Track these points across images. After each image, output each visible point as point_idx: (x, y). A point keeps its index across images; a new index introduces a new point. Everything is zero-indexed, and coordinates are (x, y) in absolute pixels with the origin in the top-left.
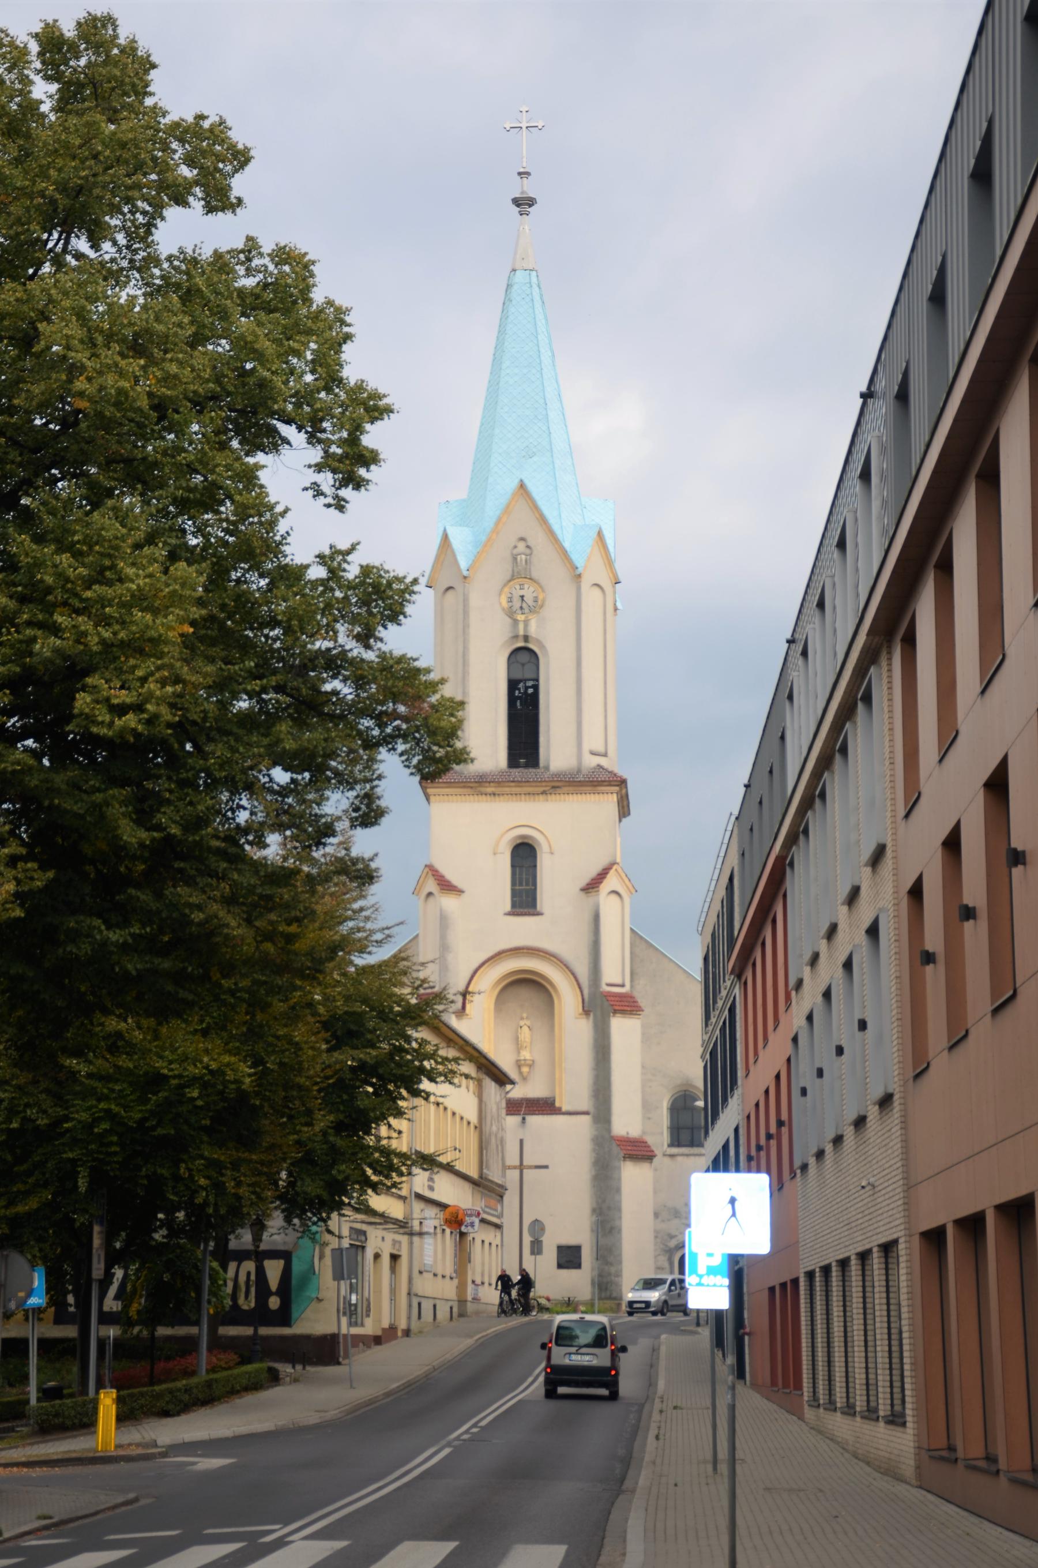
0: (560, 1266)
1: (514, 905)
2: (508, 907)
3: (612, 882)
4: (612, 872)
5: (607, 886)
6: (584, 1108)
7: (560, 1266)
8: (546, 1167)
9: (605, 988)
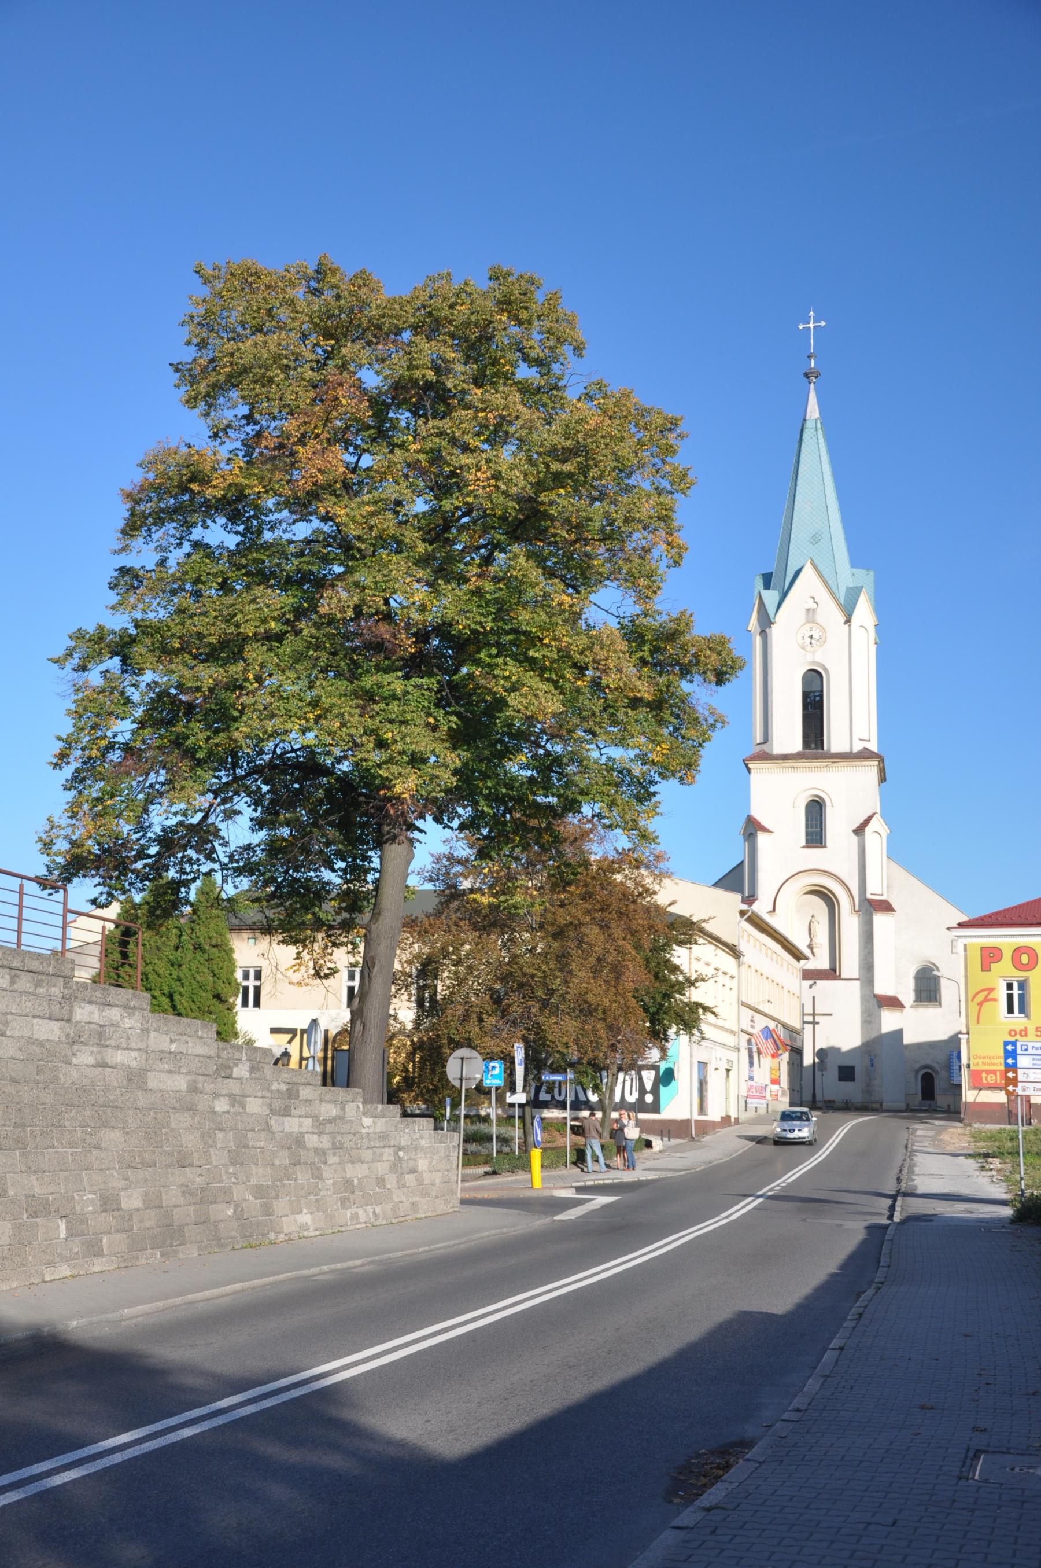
0: (841, 1079)
1: (807, 841)
2: (804, 843)
3: (876, 824)
4: (874, 819)
5: (868, 830)
6: (857, 976)
7: (841, 1079)
8: (814, 998)
9: (869, 896)
